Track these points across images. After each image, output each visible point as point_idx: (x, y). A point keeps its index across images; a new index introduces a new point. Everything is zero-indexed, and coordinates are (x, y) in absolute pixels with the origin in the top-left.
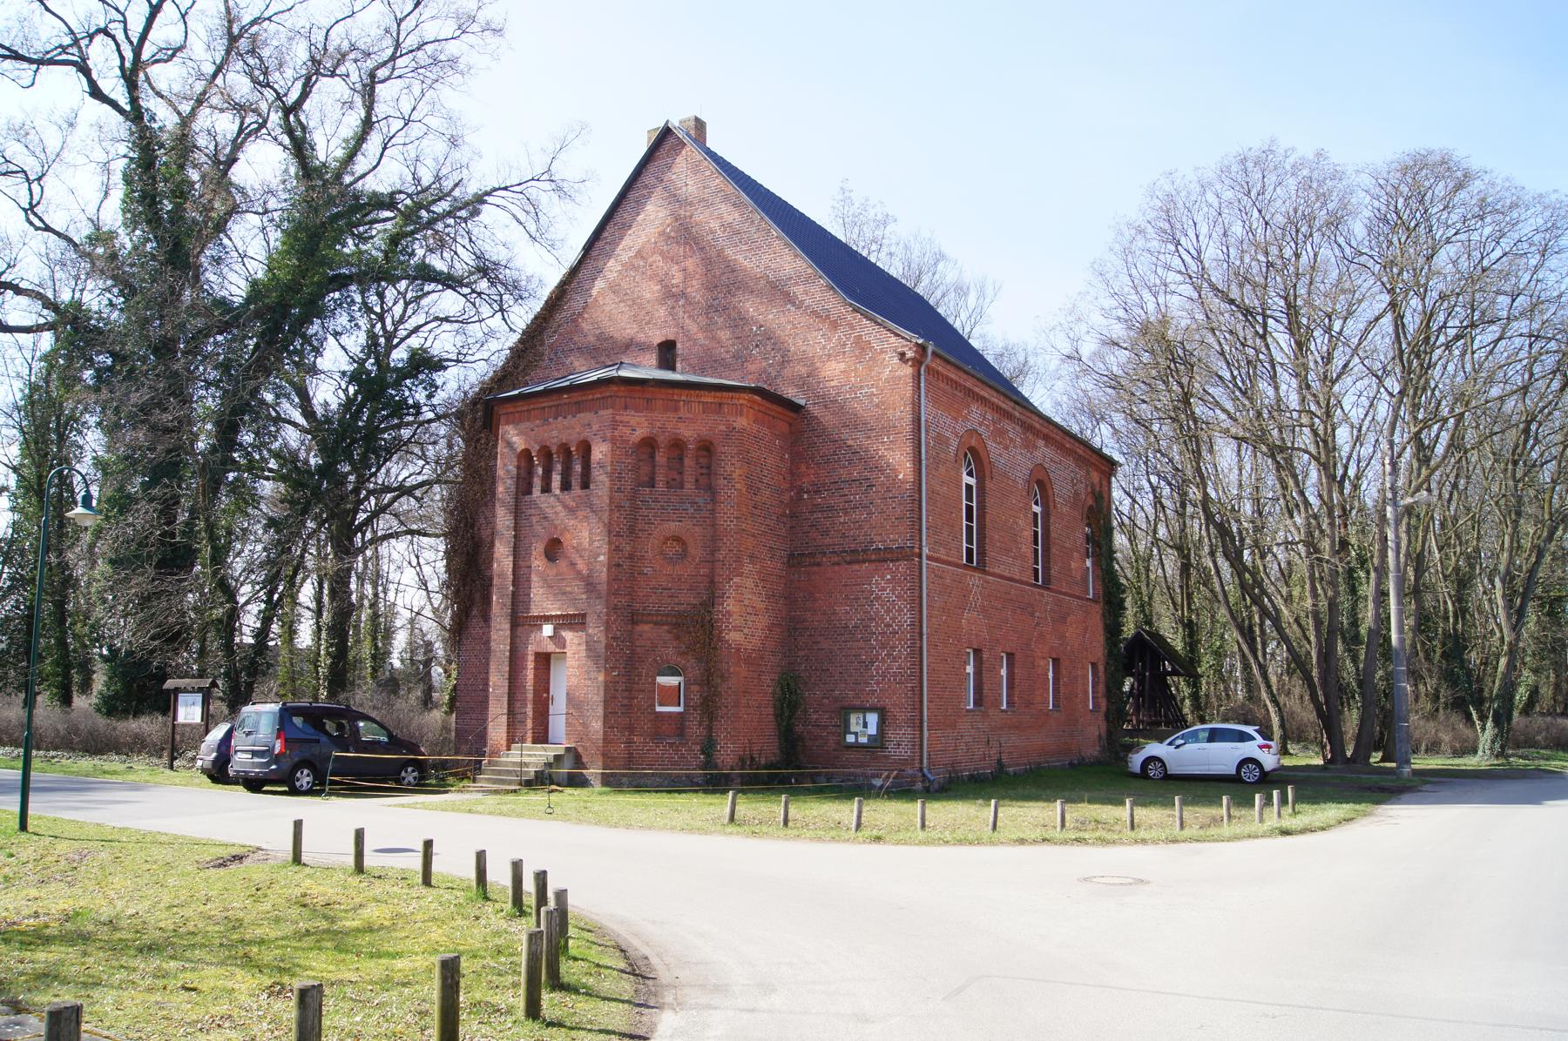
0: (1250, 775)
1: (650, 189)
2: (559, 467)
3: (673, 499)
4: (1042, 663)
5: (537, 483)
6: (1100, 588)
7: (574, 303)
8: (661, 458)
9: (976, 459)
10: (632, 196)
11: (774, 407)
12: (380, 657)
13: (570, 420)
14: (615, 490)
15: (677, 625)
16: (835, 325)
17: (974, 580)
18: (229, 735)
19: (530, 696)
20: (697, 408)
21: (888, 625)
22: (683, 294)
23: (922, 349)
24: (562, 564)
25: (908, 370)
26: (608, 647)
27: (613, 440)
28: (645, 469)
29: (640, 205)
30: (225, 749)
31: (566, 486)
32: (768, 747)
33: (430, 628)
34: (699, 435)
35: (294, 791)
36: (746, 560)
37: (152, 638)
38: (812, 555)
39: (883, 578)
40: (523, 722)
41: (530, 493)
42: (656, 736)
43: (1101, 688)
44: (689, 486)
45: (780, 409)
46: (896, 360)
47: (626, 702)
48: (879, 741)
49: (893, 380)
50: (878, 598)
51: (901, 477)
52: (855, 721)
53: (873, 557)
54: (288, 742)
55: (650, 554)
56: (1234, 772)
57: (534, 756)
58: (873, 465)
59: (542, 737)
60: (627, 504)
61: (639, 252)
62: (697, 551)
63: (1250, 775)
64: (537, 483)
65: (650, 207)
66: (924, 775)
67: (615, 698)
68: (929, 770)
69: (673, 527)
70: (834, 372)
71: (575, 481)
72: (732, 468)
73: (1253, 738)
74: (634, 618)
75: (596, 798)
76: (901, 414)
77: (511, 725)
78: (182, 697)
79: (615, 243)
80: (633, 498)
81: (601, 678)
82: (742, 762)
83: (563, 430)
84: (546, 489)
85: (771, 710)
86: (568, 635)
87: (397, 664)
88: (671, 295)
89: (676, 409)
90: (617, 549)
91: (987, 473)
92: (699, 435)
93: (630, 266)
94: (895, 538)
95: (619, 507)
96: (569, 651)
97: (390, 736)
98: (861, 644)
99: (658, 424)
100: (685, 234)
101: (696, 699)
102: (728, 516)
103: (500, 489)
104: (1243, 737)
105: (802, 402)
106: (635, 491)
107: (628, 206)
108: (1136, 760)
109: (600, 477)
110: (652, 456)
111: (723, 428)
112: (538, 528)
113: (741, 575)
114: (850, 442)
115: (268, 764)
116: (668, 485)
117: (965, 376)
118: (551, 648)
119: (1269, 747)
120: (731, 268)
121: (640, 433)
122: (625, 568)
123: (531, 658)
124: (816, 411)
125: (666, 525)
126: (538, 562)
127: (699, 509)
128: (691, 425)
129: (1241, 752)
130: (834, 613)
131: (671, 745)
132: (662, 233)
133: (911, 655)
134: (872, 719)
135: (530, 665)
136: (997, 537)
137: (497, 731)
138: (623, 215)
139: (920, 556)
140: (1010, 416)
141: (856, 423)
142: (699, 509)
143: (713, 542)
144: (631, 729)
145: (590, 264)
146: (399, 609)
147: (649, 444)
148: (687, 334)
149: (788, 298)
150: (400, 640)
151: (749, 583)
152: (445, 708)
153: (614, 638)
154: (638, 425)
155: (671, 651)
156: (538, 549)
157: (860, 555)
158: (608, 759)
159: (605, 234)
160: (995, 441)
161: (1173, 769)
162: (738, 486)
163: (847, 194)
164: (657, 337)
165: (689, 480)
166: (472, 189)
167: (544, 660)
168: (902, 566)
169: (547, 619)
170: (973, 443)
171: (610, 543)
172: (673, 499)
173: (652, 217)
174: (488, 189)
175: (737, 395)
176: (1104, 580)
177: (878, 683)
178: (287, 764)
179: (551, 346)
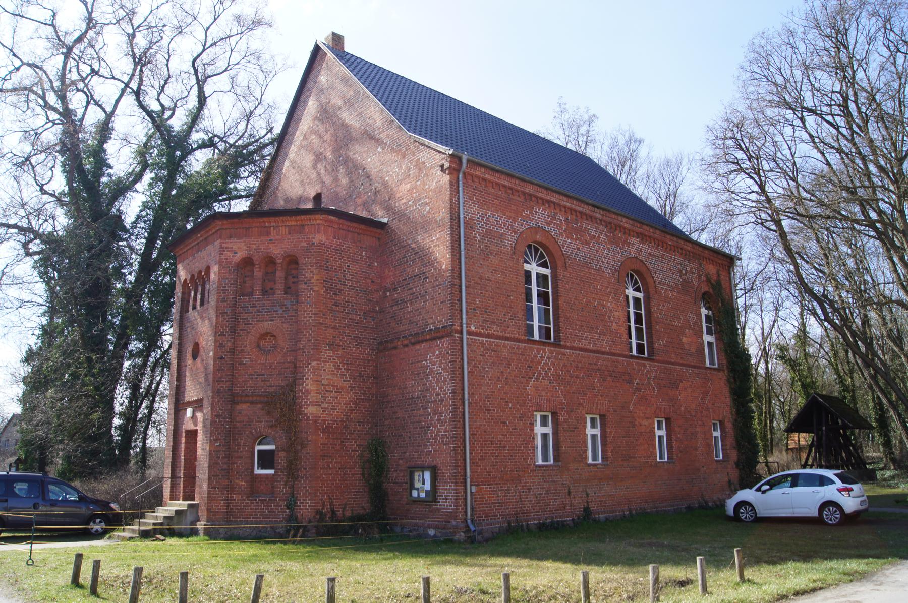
0: (831, 517)
3: (266, 303)
4: (645, 422)
8: (258, 273)
11: (354, 225)
20: (284, 231)
21: (438, 395)
25: (447, 178)
34: (285, 252)
38: (392, 341)
39: (434, 353)
43: (731, 441)
44: (279, 293)
45: (363, 227)
46: (439, 173)
47: (225, 467)
49: (439, 189)
51: (444, 267)
53: (428, 337)
55: (248, 349)
56: (816, 514)
58: (423, 256)
60: (229, 310)
63: (831, 517)
66: (467, 526)
67: (217, 464)
68: (472, 520)
69: (266, 325)
72: (311, 274)
73: (833, 482)
76: (442, 214)
80: (235, 305)
82: (320, 515)
84: (194, 308)
85: (358, 471)
89: (268, 234)
92: (285, 252)
94: (440, 319)
98: (421, 412)
99: (254, 247)
104: (823, 481)
105: (385, 220)
108: (731, 504)
111: (304, 244)
113: (319, 359)
114: (413, 245)
117: (522, 183)
119: (849, 490)
121: (240, 255)
124: (394, 225)
126: (189, 361)
129: (820, 495)
130: (405, 388)
131: (263, 501)
133: (454, 418)
134: (427, 475)
136: (575, 316)
139: (461, 332)
140: (590, 218)
142: (287, 310)
147: (248, 262)
151: (329, 366)
153: (218, 416)
154: (239, 249)
155: (263, 424)
161: (762, 512)
162: (316, 289)
163: (563, 106)
167: (192, 434)
168: (445, 343)
170: (539, 238)
171: (216, 341)
172: (266, 303)
173: (311, 106)
175: (312, 217)
176: (726, 352)
177: (432, 445)
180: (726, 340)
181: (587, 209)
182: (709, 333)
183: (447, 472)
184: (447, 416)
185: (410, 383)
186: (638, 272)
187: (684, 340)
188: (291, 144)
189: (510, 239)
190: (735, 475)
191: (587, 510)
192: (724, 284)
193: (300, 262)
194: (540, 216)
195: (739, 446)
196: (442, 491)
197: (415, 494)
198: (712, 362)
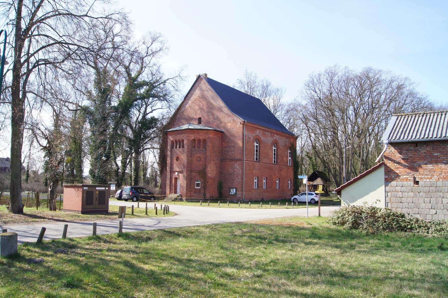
0: (313, 202)
1: (197, 87)
2: (178, 144)
4: (275, 179)
5: (175, 146)
6: (292, 163)
7: (183, 109)
8: (196, 143)
9: (258, 140)
10: (193, 88)
12: (145, 175)
13: (180, 136)
14: (188, 148)
15: (199, 173)
16: (229, 116)
17: (257, 164)
18: (122, 192)
19: (173, 185)
20: (203, 133)
22: (203, 109)
23: (244, 122)
24: (179, 161)
25: (241, 126)
26: (187, 177)
27: (188, 140)
28: (193, 144)
29: (195, 90)
30: (121, 194)
31: (180, 147)
32: (216, 195)
33: (156, 166)
35: (133, 201)
36: (212, 161)
37: (104, 174)
40: (172, 190)
41: (173, 148)
42: (195, 192)
43: (292, 184)
44: (201, 148)
46: (240, 124)
48: (236, 194)
49: (239, 127)
50: (236, 168)
52: (232, 190)
54: (132, 193)
57: (174, 196)
58: (235, 143)
59: (176, 192)
61: (195, 100)
62: (203, 159)
64: (175, 146)
65: (196, 91)
69: (198, 155)
70: (229, 125)
71: (181, 147)
72: (209, 144)
73: (314, 195)
74: (191, 171)
75: (185, 203)
77: (170, 190)
78: (111, 185)
79: (190, 98)
81: (186, 182)
83: (179, 137)
84: (176, 148)
85: (217, 188)
86: (180, 174)
87: (149, 176)
88: (201, 109)
89: (199, 134)
90: (188, 159)
91: (261, 143)
93: (193, 102)
94: (238, 157)
95: (189, 152)
96: (180, 177)
97: (149, 192)
100: (203, 97)
101: (203, 186)
102: (208, 153)
103: (168, 147)
105: (223, 131)
106: (192, 149)
107: (193, 90)
108: (292, 198)
109: (186, 147)
110: (195, 142)
112: (175, 155)
115: (129, 197)
116: (198, 147)
118: (177, 177)
119: (317, 196)
120: (212, 104)
121: (192, 138)
122: (190, 163)
123: (174, 178)
124: (226, 132)
125: (197, 155)
126: (175, 161)
127: (203, 152)
128: (202, 137)
132: (199, 96)
134: (234, 190)
135: (174, 180)
137: (168, 191)
138: (191, 92)
140: (267, 131)
141: (233, 135)
142: (203, 152)
143: (206, 158)
144: (191, 191)
145: (185, 102)
146: (149, 162)
147: (194, 140)
148: (204, 117)
149: (221, 111)
150: (149, 171)
151: (212, 165)
152: (159, 187)
154: (192, 137)
155: (198, 177)
156: (175, 159)
157: (233, 160)
158: (186, 196)
159: (188, 96)
160: (263, 136)
164: (198, 117)
165: (201, 146)
166: (164, 78)
167: (176, 179)
168: (240, 162)
169: (176, 171)
170: (257, 137)
173: (197, 93)
174: (167, 79)
178: (132, 196)
179: (178, 117)
180: (294, 158)
181: (266, 129)
182: (290, 157)
183: (239, 189)
184: (240, 177)
185: (230, 170)
186: (276, 143)
187: (284, 159)
188: (189, 100)
189: (252, 138)
190: (292, 193)
191: (263, 198)
192: (295, 144)
193: (207, 141)
194: (258, 132)
195: (294, 185)
196: (238, 193)
197: (231, 193)
198: (290, 164)
